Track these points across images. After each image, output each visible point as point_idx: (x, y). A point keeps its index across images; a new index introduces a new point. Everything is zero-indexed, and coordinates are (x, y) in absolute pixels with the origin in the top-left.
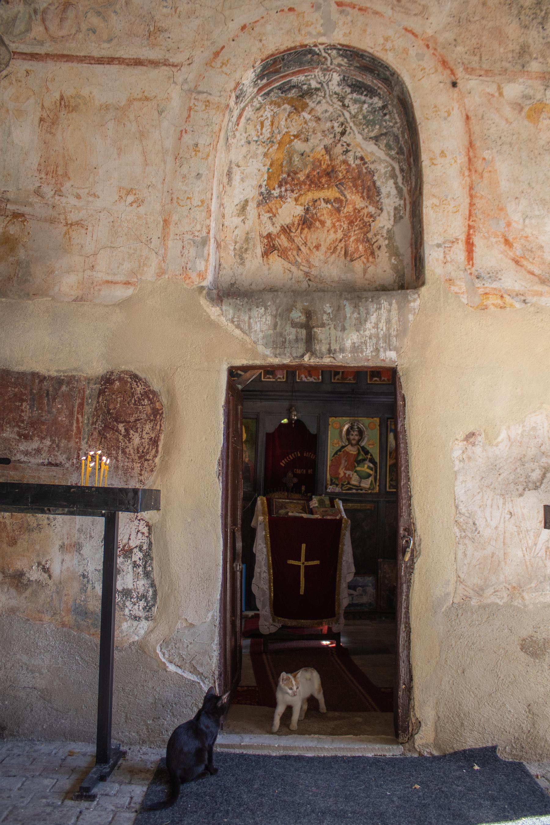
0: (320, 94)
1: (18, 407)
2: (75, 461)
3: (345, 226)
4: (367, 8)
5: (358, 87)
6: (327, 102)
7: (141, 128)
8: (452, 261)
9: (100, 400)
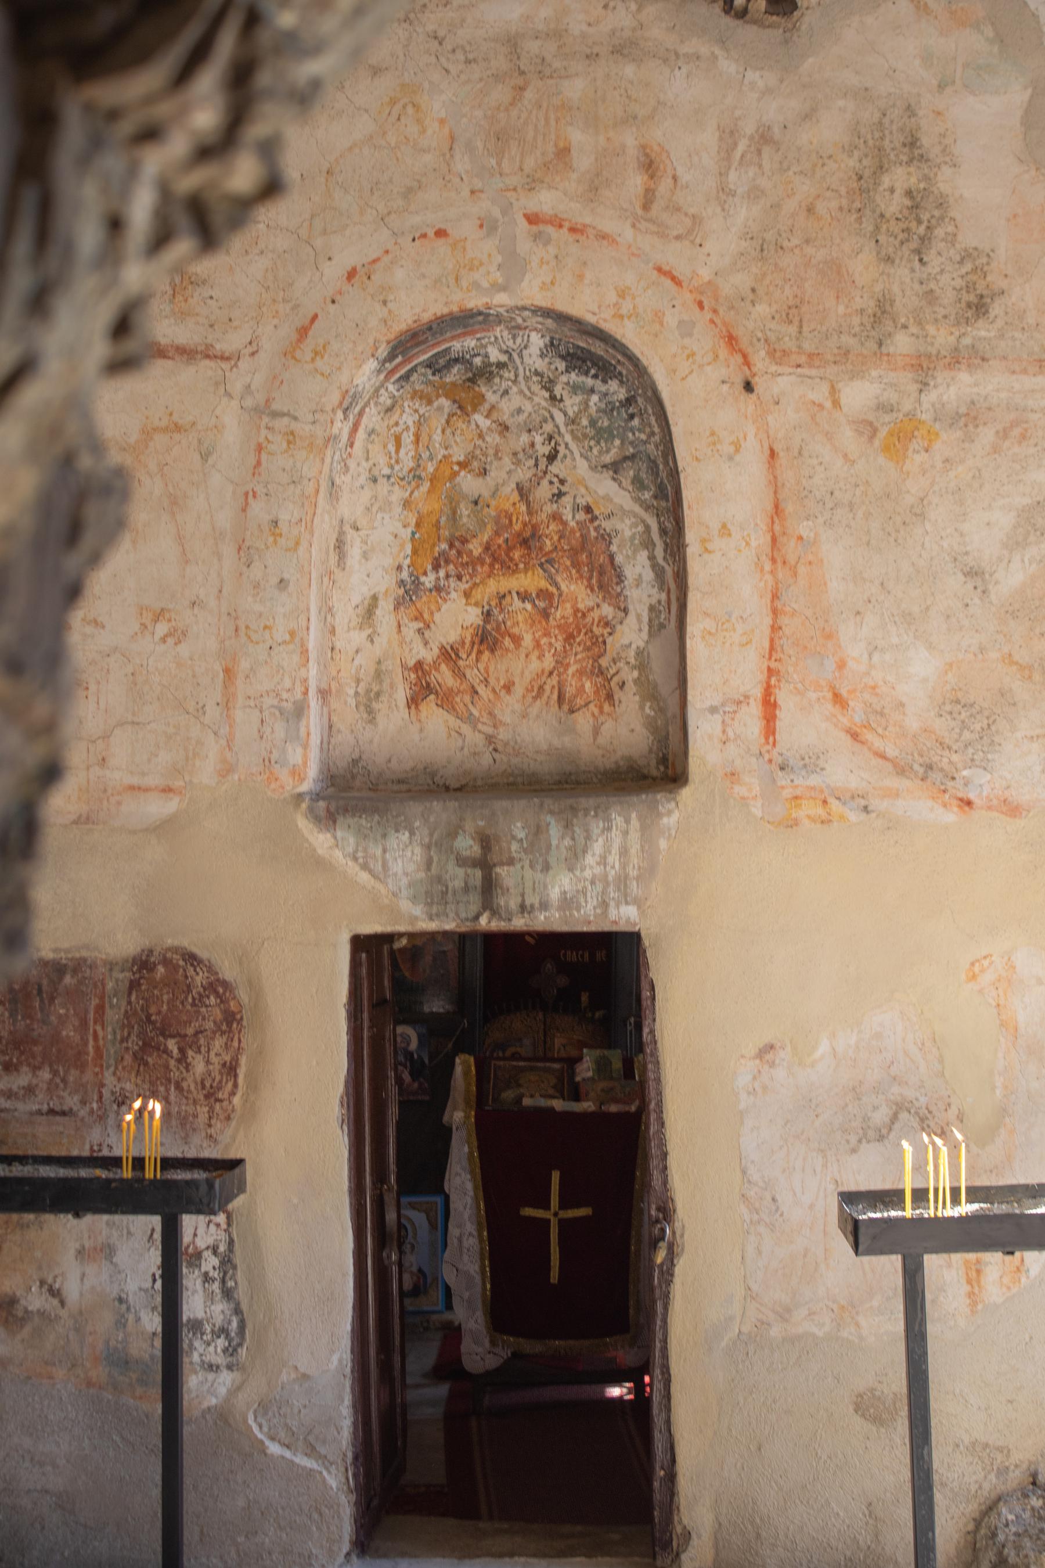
0: (506, 375)
3: (559, 645)
4: (585, 226)
5: (578, 358)
6: (521, 392)
8: (737, 737)
9: (133, 998)
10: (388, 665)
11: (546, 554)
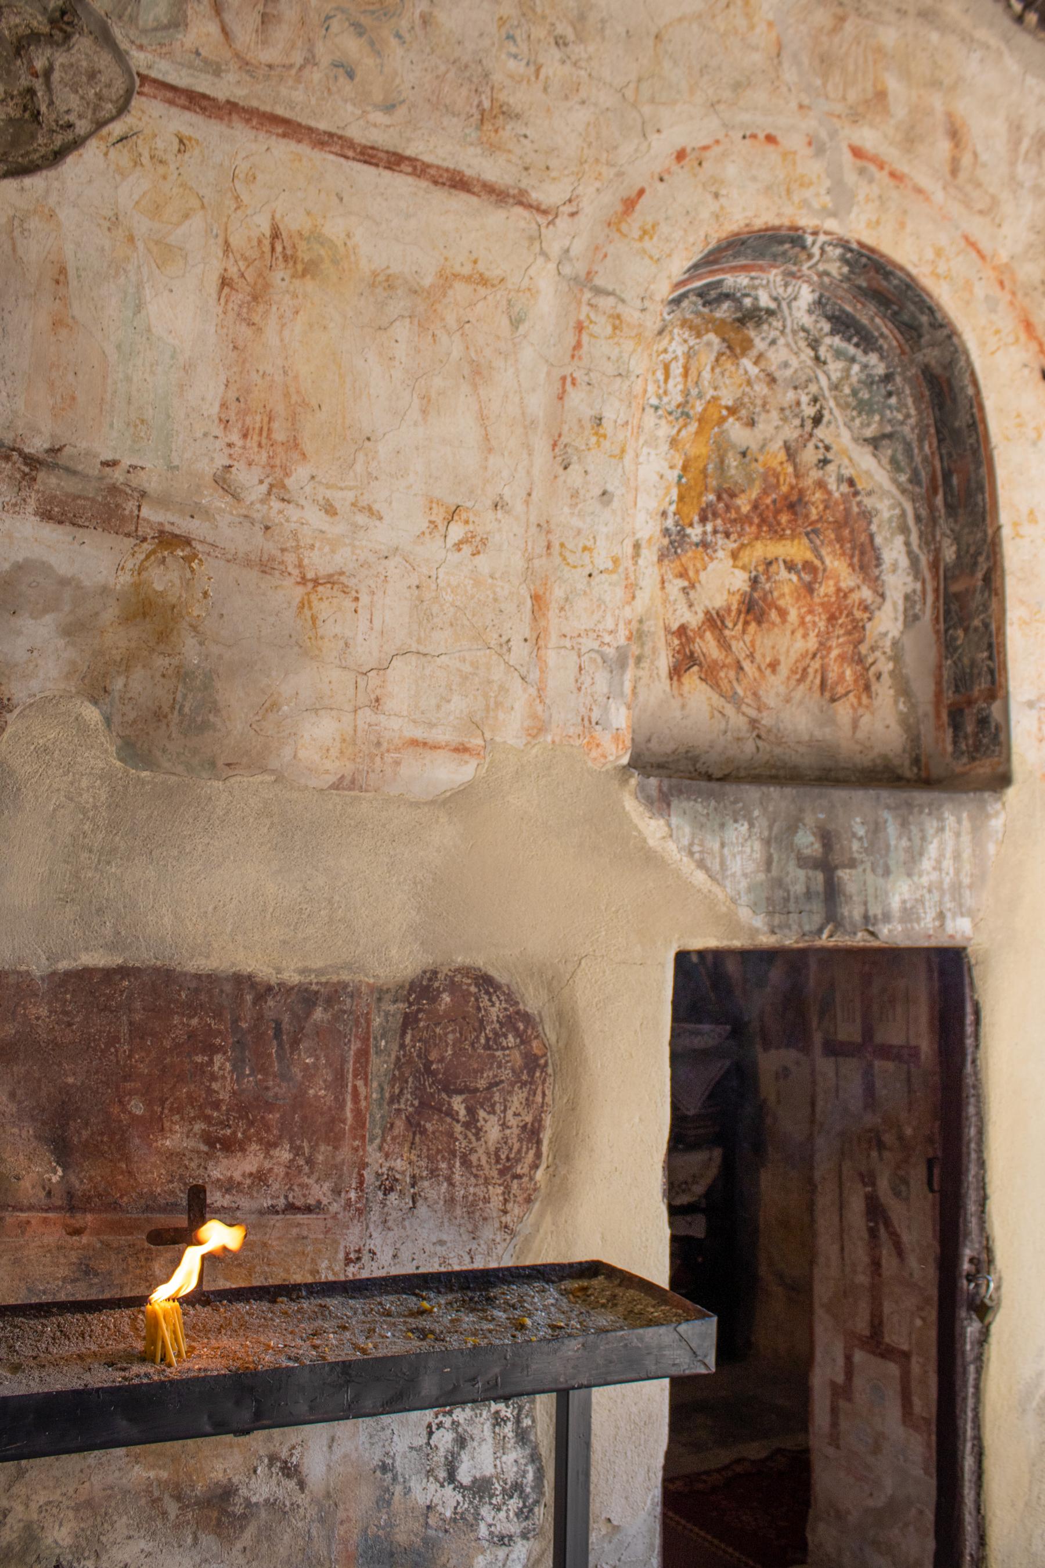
0: (775, 323)
1: (201, 1069)
2: (353, 1195)
3: (822, 625)
5: (843, 323)
7: (473, 355)
9: (408, 1039)
10: (650, 626)
11: (811, 524)
